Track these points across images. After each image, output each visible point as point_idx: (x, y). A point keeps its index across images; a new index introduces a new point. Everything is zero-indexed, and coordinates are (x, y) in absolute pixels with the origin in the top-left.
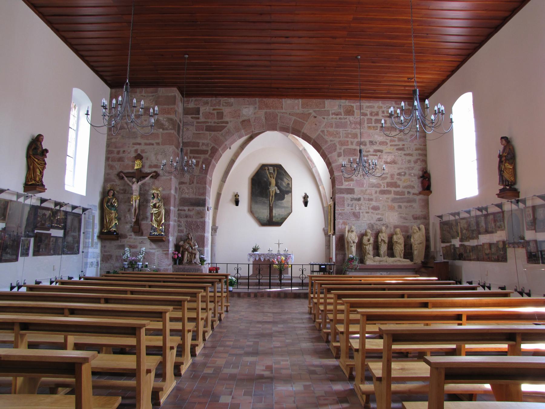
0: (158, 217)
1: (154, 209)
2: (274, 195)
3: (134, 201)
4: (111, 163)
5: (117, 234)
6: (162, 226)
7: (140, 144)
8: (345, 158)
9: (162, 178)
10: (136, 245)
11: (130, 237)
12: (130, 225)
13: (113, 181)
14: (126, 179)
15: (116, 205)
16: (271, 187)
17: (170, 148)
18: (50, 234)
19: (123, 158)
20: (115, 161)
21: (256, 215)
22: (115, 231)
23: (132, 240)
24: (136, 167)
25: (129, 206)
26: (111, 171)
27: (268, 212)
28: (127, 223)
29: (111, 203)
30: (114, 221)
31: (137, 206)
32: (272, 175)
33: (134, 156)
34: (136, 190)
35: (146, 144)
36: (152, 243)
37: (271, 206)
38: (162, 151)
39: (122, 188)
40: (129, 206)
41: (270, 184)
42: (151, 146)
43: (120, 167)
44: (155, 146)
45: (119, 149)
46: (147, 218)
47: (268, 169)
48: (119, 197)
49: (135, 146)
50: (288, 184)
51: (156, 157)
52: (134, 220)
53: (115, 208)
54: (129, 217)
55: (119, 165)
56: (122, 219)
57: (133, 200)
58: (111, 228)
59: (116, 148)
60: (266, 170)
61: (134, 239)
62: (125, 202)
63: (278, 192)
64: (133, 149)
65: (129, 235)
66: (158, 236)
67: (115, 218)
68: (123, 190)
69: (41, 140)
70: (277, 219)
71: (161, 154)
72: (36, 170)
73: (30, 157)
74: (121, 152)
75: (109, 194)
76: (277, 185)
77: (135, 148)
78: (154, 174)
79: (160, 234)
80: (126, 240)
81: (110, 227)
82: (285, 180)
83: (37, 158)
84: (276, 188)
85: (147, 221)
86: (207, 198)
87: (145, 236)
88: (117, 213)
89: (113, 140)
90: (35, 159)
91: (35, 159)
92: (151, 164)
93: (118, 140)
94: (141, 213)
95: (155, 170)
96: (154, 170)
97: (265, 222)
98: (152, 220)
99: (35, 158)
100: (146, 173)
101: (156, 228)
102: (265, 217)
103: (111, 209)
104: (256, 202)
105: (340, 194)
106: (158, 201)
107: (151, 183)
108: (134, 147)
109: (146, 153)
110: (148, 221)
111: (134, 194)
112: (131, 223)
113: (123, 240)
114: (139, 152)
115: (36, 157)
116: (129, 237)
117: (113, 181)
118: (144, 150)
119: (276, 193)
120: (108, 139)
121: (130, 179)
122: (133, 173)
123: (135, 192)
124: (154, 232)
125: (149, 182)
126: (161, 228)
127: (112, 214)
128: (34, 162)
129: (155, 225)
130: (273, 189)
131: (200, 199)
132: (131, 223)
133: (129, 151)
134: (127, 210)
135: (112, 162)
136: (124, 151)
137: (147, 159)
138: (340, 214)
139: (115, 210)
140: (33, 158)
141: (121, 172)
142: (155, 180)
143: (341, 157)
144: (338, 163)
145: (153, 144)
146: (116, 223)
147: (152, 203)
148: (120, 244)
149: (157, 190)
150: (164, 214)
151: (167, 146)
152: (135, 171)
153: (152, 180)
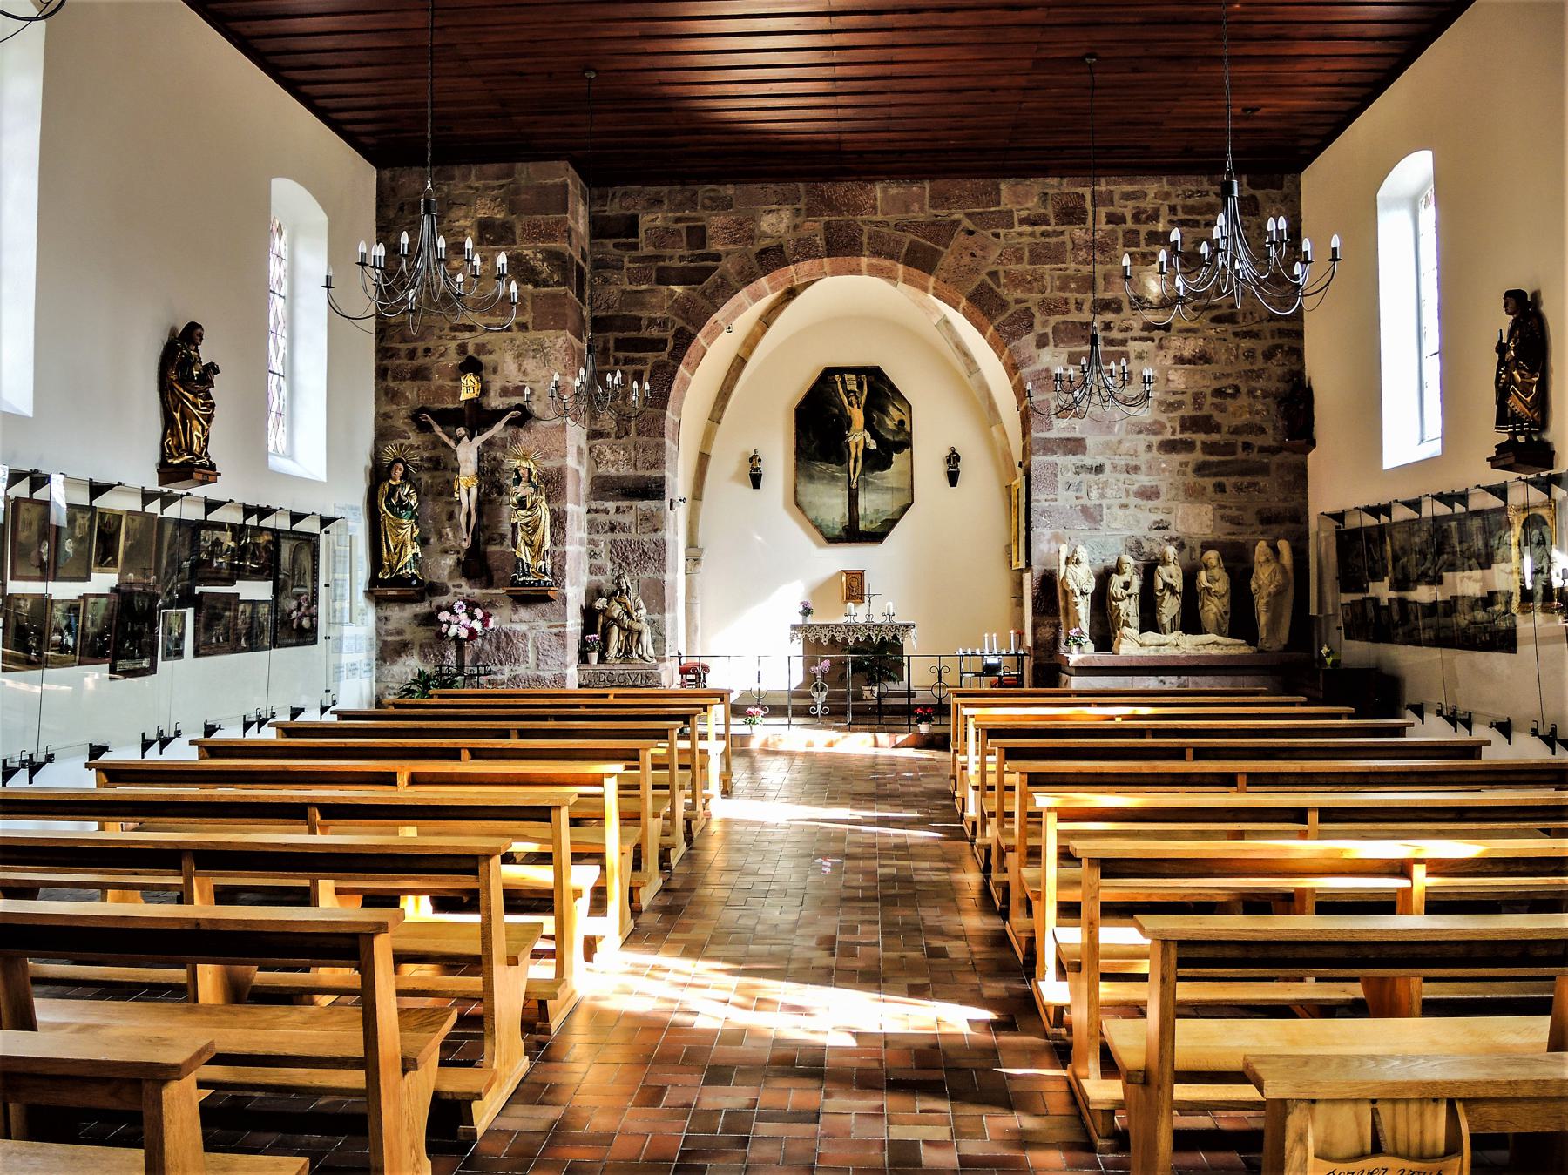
0: (532, 535)
2: (860, 455)
3: (463, 491)
7: (471, 328)
8: (1059, 349)
11: (457, 590)
16: (852, 432)
19: (426, 368)
20: (405, 380)
21: (812, 515)
26: (395, 407)
27: (844, 503)
32: (853, 399)
37: (854, 486)
38: (535, 347)
39: (426, 455)
41: (849, 422)
43: (418, 395)
44: (516, 333)
47: (843, 382)
48: (420, 479)
49: (457, 334)
50: (902, 422)
51: (520, 365)
54: (450, 535)
55: (416, 389)
56: (432, 540)
58: (401, 569)
59: (404, 341)
60: (836, 382)
63: (873, 446)
64: (453, 344)
65: (454, 586)
66: (533, 585)
68: (430, 460)
70: (872, 522)
71: (534, 357)
74: (420, 352)
76: (868, 425)
81: (400, 566)
82: (891, 409)
84: (867, 434)
88: (418, 526)
90: (186, 393)
91: (186, 393)
92: (507, 384)
96: (516, 400)
97: (837, 532)
102: (837, 519)
104: (811, 478)
105: (1045, 454)
109: (491, 352)
112: (458, 553)
115: (189, 387)
116: (453, 590)
118: (484, 345)
119: (866, 450)
125: (503, 435)
129: (524, 558)
130: (857, 439)
131: (649, 478)
134: (444, 517)
135: (394, 380)
136: (427, 350)
137: (495, 371)
138: (1044, 512)
141: (424, 409)
142: (521, 430)
143: (1046, 348)
144: (1039, 366)
146: (415, 555)
152: (463, 405)
153: (511, 430)
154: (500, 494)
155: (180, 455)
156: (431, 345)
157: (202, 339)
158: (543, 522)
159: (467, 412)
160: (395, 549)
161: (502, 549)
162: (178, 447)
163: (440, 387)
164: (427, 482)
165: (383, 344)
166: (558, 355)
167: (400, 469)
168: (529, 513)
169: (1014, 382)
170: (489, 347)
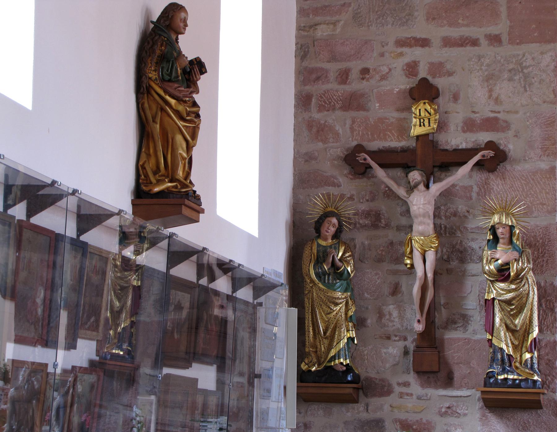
0: (515, 316)
1: (502, 285)
3: (417, 256)
4: (316, 116)
5: (357, 379)
6: (531, 352)
7: (424, 43)
9: (518, 168)
10: (429, 423)
11: (404, 390)
12: (401, 344)
13: (328, 182)
14: (380, 173)
15: (349, 269)
17: (542, 53)
18: (196, 381)
19: (362, 95)
20: (334, 109)
22: (349, 369)
23: (410, 403)
24: (417, 131)
25: (395, 273)
26: (320, 145)
28: (389, 338)
29: (333, 264)
30: (344, 329)
31: (430, 275)
33: (403, 87)
34: (424, 216)
35: (448, 42)
36: (490, 416)
38: (511, 66)
39: (363, 207)
40: (395, 273)
42: (469, 48)
43: (352, 129)
44: (485, 48)
45: (343, 65)
46: (465, 319)
48: (353, 239)
49: (405, 50)
51: (490, 91)
52: (419, 328)
53: (345, 283)
54: (395, 314)
55: (349, 122)
56: (369, 321)
57: (415, 252)
58: (333, 358)
59: (333, 58)
61: (419, 398)
62: (380, 260)
64: (399, 64)
65: (399, 384)
66: (519, 386)
67: (349, 319)
68: (367, 214)
69: (182, 25)
71: (510, 80)
72: (173, 139)
73: (149, 89)
74: (354, 74)
75: (323, 230)
77: (407, 59)
78: (490, 153)
79: (526, 380)
80: (386, 402)
81: (333, 353)
83: (177, 94)
85: (465, 330)
86: (216, 256)
87: (459, 388)
88: (354, 302)
89: (322, 32)
90: (168, 98)
91: (168, 98)
92: (473, 116)
93: (338, 30)
94: (442, 302)
95: (488, 139)
96: (484, 137)
98: (490, 328)
99: (166, 92)
100: (455, 150)
101: (509, 356)
103: (331, 287)
106: (516, 254)
107: (475, 189)
108: (401, 54)
109: (450, 74)
110: (470, 328)
111: (417, 228)
112: (405, 339)
113: (374, 402)
114: (423, 73)
115: (171, 91)
116: (398, 389)
117: (328, 182)
118: (441, 65)
120: (299, 29)
121: (399, 172)
122: (404, 150)
123: (421, 223)
124: (504, 371)
125: (467, 182)
126: (528, 356)
127: (336, 304)
128: (163, 110)
129: (505, 347)
132: (405, 339)
133: (385, 69)
134: (386, 290)
135: (320, 111)
136: (365, 71)
137: (456, 98)
139: (346, 291)
140: (162, 93)
141: (360, 148)
142: (492, 176)
145: (475, 43)
146: (351, 339)
147: (489, 262)
148: (364, 416)
149: (505, 210)
150: (536, 304)
151: (534, 46)
152: (412, 144)
153: (480, 176)
154: (462, 261)
155: (159, 182)
156: (369, 64)
157: (186, 25)
158: (530, 299)
159: (419, 152)
160: (325, 333)
161: (466, 336)
162: (156, 171)
163: (381, 120)
164: (363, 244)
165: (305, 64)
166: (544, 76)
167: (334, 225)
168: (513, 287)
169: (210, 289)
170: (448, 66)
